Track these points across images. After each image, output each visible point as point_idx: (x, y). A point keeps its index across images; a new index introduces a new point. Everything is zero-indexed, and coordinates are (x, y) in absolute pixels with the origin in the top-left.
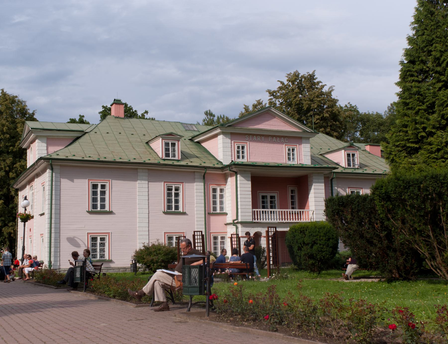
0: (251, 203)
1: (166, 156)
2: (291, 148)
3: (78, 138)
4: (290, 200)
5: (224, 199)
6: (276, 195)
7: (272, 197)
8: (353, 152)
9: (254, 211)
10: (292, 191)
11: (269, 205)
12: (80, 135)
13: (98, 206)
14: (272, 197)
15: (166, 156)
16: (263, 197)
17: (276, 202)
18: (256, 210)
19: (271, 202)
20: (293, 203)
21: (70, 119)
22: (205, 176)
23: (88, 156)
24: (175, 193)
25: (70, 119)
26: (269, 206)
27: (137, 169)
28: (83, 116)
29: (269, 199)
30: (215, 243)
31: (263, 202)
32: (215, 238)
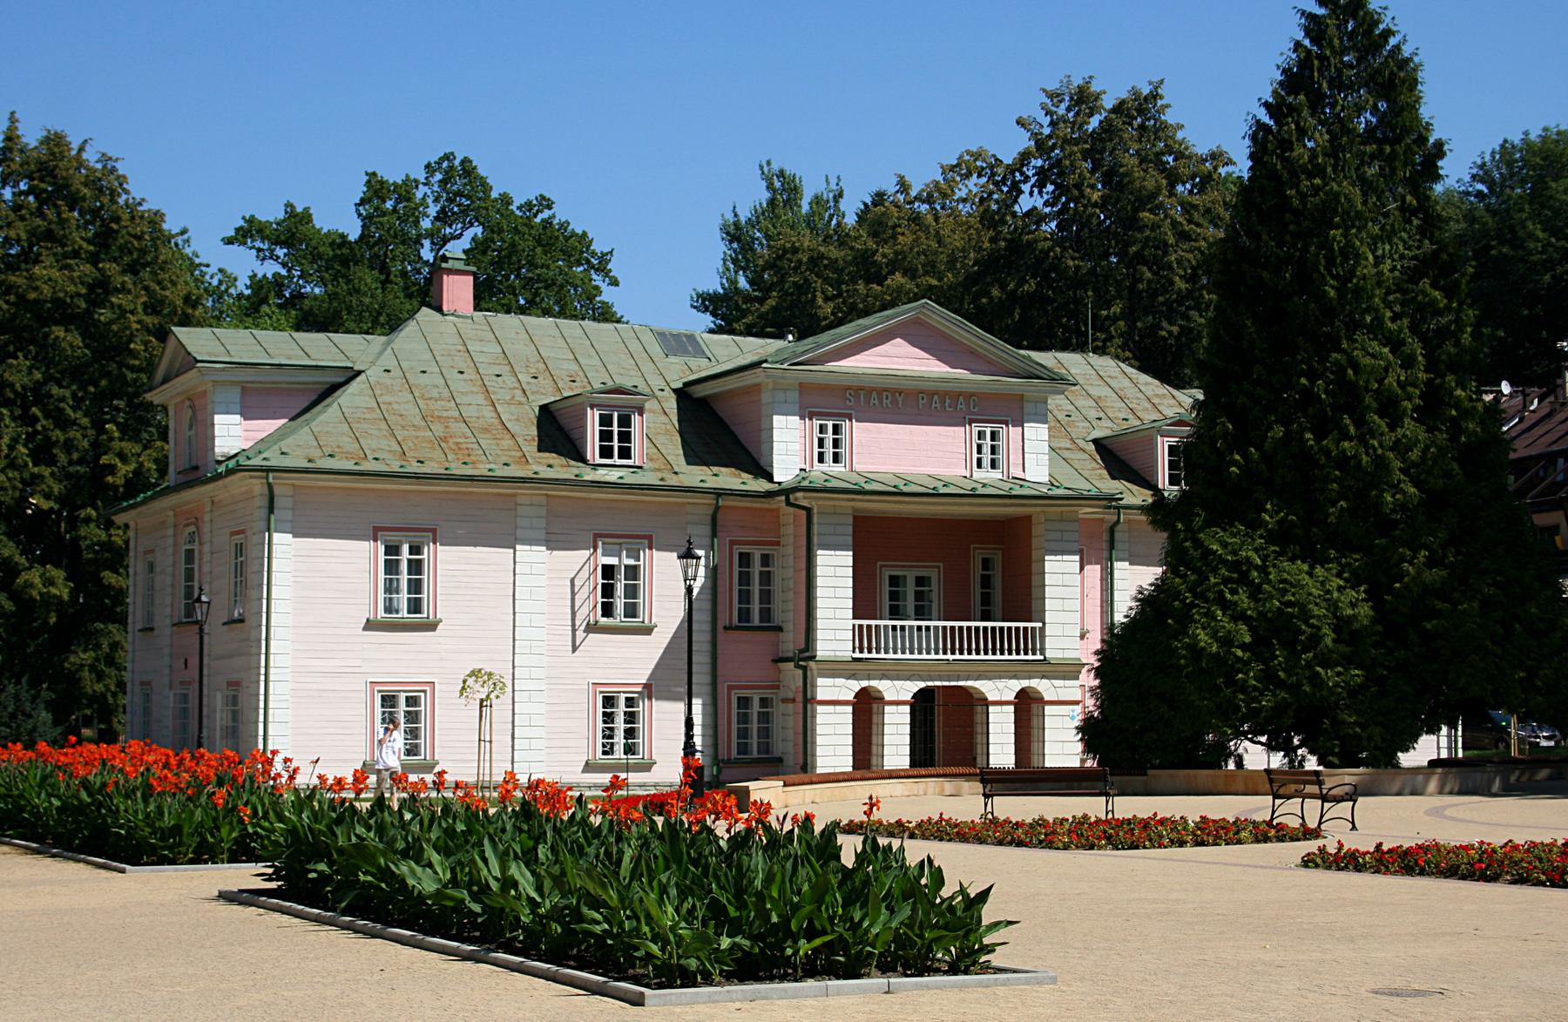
0: (850, 603)
1: (602, 456)
2: (988, 431)
3: (333, 389)
4: (978, 590)
5: (776, 587)
6: (933, 574)
7: (920, 581)
8: (978, 475)
9: (861, 626)
10: (986, 564)
11: (910, 604)
12: (342, 380)
13: (406, 608)
14: (920, 581)
15: (602, 456)
16: (894, 581)
17: (934, 596)
18: (865, 622)
19: (919, 596)
20: (986, 599)
21: (307, 210)
22: (719, 516)
23: (328, 451)
24: (761, 573)
25: (307, 210)
26: (911, 609)
27: (514, 495)
28: (374, 174)
29: (910, 589)
30: (744, 719)
31: (894, 596)
32: (744, 702)
